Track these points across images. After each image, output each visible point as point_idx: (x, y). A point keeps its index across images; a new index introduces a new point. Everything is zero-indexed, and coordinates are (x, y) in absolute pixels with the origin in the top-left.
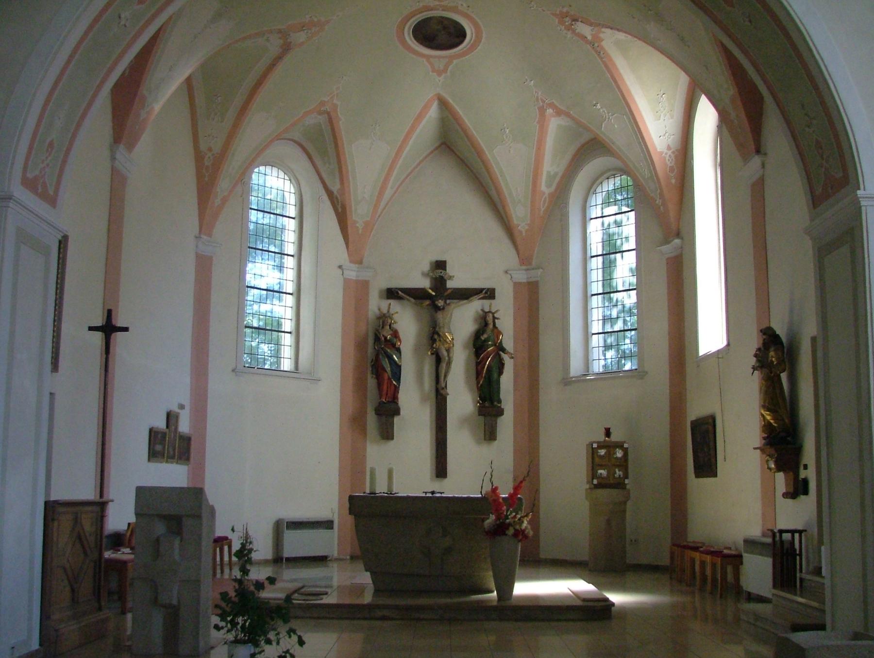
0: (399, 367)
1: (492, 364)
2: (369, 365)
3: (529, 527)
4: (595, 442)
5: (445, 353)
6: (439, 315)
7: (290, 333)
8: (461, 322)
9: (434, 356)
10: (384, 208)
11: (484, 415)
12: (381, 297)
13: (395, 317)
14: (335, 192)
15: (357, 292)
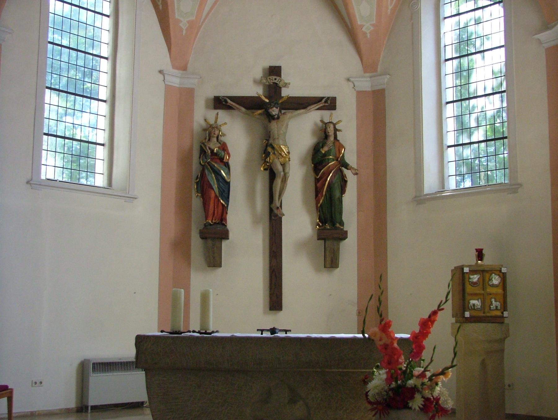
0: (228, 184)
1: (334, 181)
2: (194, 181)
3: (446, 393)
5: (280, 168)
6: (274, 125)
7: (103, 145)
8: (298, 135)
9: (267, 173)
10: (210, 11)
11: (324, 239)
12: (207, 107)
13: (224, 129)
15: (180, 101)
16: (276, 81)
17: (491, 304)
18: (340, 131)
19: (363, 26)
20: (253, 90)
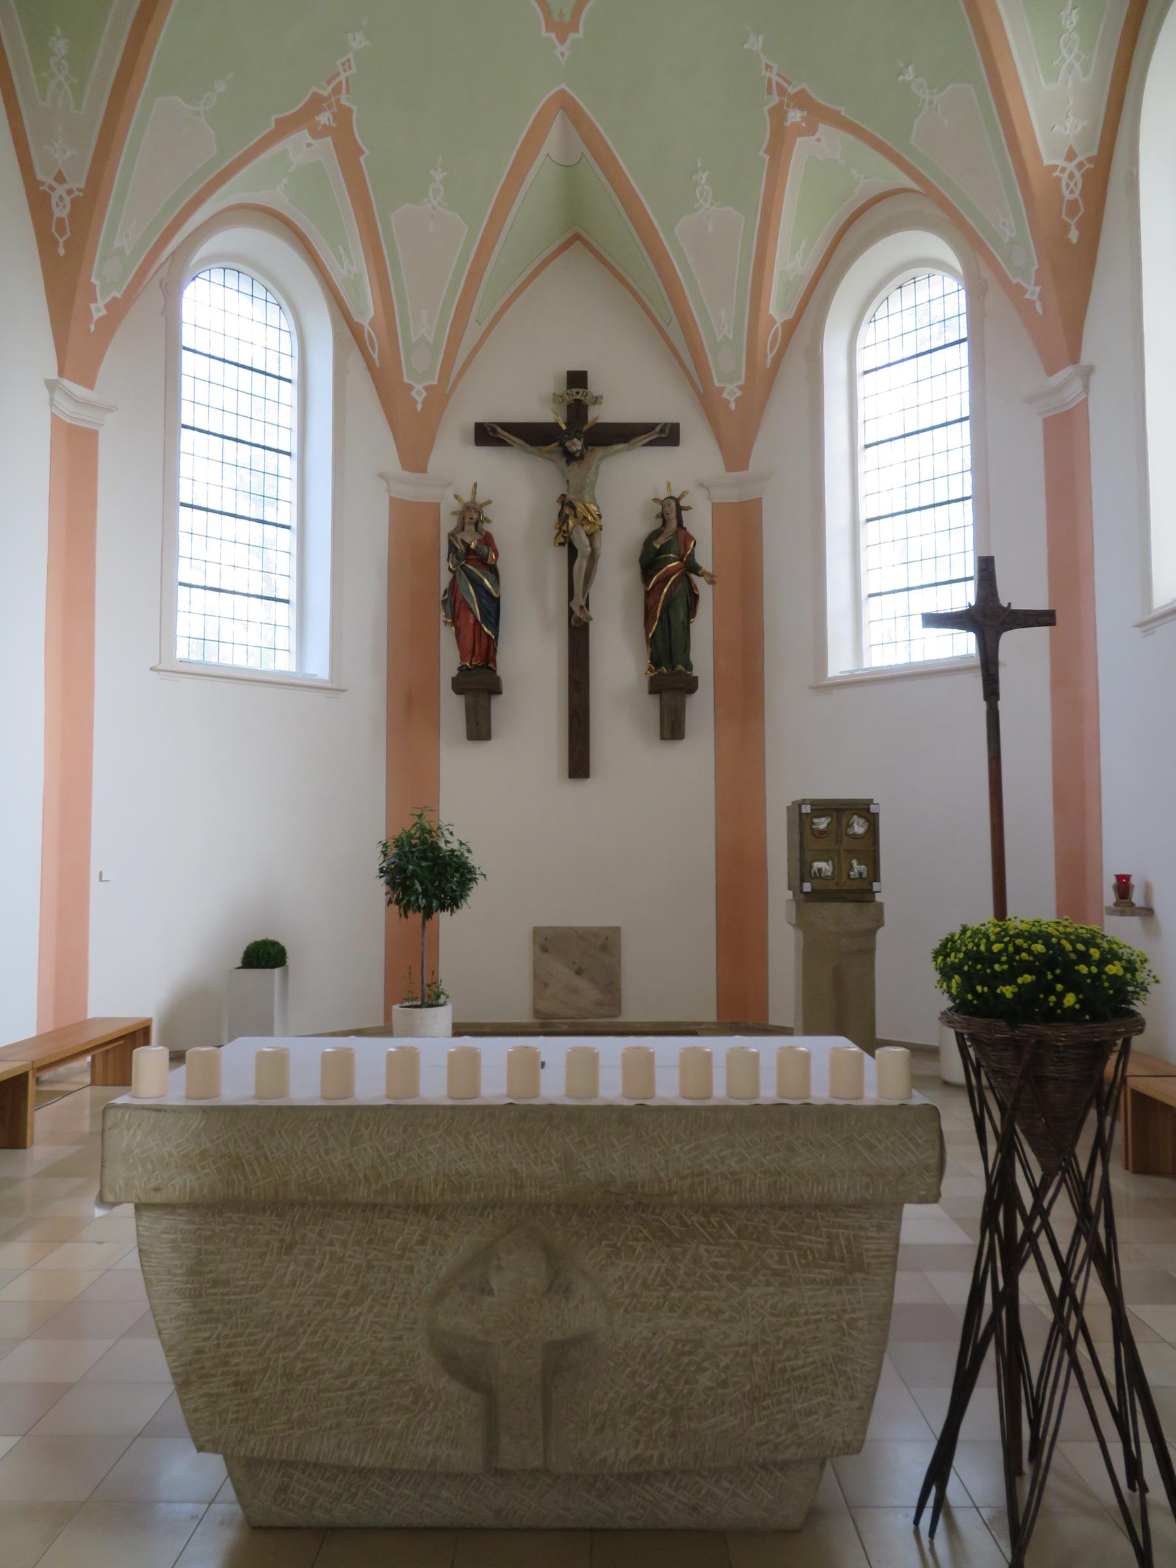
0: (497, 601)
4: (804, 802)
5: (586, 541)
14: (367, 327)
16: (578, 397)
17: (851, 868)
18: (687, 509)
19: (723, 389)
20: (545, 413)
